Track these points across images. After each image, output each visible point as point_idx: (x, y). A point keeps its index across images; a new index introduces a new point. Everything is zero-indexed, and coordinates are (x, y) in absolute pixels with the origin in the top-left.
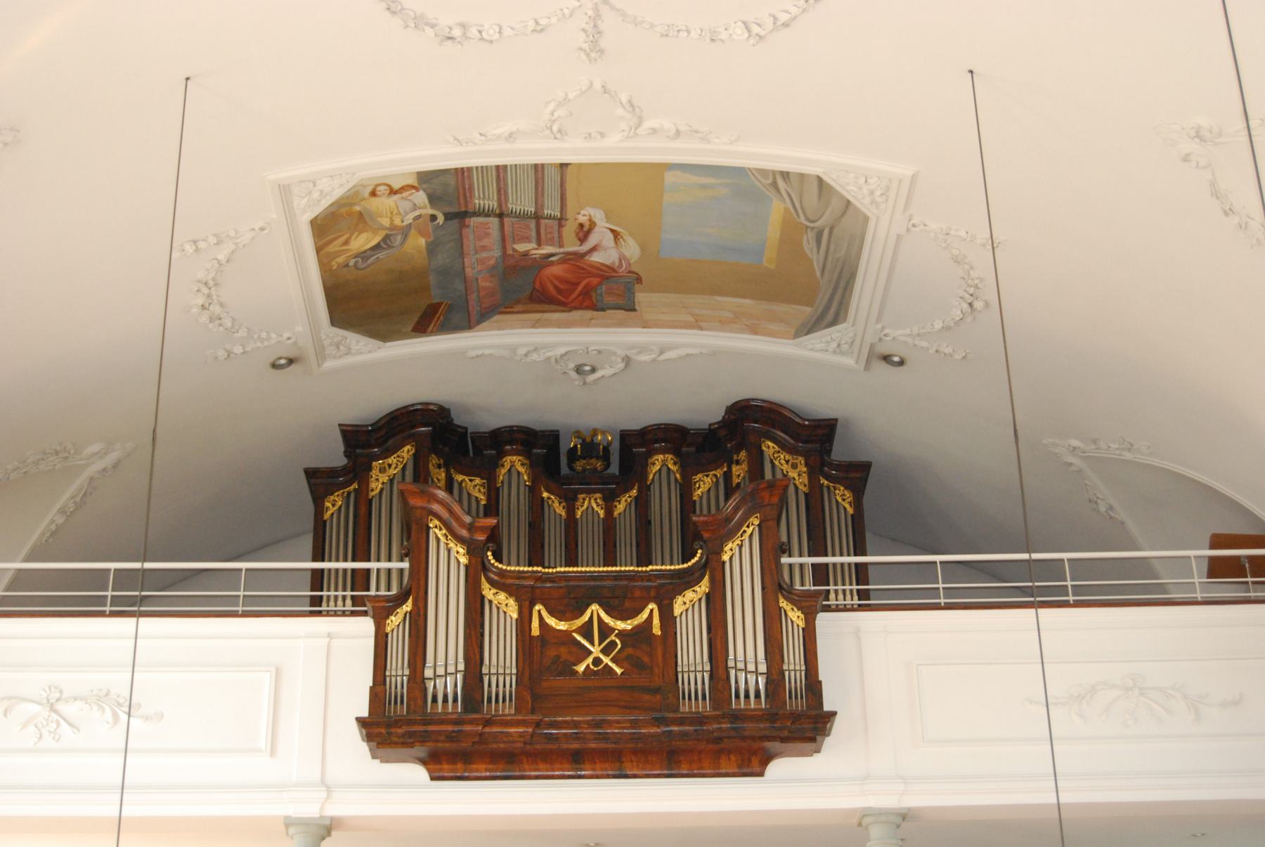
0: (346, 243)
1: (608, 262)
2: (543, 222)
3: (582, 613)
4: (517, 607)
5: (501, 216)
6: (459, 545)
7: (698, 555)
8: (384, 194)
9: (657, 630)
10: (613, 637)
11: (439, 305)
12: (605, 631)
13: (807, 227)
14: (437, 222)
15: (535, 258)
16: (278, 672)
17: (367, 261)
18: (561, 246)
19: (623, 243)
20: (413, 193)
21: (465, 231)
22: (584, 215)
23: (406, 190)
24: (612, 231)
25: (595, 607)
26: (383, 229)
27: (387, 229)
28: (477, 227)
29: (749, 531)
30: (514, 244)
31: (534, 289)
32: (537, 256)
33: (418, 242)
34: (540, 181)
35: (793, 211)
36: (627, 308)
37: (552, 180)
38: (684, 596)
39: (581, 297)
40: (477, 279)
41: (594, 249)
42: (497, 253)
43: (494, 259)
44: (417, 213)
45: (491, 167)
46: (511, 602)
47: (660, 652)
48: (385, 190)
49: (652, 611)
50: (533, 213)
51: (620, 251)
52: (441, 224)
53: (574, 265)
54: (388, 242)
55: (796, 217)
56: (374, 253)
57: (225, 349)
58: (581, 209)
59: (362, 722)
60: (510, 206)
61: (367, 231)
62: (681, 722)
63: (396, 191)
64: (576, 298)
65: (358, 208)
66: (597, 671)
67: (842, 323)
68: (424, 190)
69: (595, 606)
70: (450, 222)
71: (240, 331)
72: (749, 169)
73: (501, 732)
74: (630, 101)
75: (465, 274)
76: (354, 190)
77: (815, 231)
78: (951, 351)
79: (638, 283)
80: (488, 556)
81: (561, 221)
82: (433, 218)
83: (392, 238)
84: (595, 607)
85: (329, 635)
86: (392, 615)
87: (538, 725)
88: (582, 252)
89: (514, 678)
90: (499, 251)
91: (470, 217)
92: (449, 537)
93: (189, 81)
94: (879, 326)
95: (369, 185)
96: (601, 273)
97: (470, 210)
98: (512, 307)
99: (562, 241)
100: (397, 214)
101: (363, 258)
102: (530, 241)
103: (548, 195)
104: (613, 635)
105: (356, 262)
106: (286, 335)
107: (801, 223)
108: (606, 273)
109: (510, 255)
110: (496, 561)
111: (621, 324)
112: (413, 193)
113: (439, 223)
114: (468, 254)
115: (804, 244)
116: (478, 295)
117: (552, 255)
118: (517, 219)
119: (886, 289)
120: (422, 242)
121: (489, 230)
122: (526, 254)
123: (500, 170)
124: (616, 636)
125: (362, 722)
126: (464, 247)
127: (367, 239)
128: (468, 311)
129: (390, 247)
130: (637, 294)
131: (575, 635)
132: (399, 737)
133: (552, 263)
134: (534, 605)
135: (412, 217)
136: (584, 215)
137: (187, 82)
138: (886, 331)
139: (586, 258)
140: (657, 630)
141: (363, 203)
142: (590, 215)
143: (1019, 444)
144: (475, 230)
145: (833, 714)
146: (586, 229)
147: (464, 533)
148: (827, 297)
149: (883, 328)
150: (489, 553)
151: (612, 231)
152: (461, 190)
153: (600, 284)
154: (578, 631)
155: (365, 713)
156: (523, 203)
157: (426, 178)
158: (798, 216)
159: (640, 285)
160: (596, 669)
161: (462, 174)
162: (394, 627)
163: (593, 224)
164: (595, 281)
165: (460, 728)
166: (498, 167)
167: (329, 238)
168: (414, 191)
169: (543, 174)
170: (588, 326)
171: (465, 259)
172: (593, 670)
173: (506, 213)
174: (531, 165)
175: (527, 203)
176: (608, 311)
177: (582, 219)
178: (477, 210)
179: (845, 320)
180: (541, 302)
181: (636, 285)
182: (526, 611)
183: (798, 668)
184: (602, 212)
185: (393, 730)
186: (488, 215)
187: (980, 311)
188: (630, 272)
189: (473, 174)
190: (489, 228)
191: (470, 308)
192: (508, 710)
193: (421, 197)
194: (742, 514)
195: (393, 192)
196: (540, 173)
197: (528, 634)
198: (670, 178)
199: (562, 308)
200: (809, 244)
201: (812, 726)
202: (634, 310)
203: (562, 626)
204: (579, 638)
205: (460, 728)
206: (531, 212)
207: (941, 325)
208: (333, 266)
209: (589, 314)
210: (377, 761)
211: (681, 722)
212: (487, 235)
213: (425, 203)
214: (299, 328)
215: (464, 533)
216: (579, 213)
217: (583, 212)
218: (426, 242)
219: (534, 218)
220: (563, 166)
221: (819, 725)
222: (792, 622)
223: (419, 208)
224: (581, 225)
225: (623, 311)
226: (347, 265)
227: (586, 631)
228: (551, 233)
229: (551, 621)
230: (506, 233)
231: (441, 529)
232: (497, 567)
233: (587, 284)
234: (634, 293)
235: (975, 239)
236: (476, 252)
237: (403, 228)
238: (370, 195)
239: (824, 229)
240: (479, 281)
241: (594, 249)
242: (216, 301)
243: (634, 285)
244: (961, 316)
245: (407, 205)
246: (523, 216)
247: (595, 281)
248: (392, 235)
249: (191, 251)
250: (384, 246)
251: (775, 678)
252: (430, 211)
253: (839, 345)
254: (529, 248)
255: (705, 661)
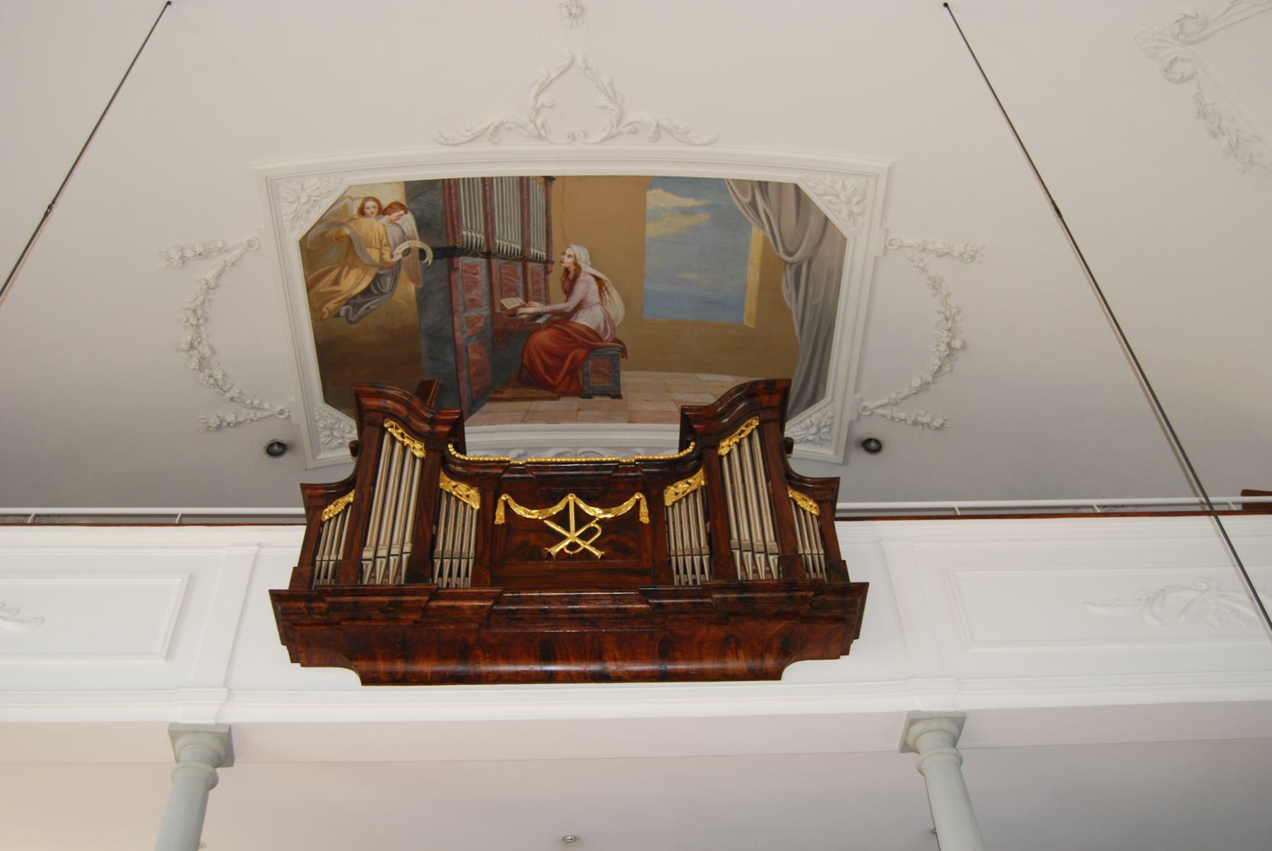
0: (336, 281)
1: (593, 327)
2: (531, 265)
3: (555, 503)
4: (479, 497)
5: (488, 255)
6: (416, 442)
7: (691, 447)
8: (372, 213)
9: (645, 519)
10: (592, 525)
11: (431, 383)
12: (582, 518)
13: (786, 263)
14: (425, 261)
15: (523, 319)
16: (192, 579)
17: (358, 310)
18: (548, 303)
19: (607, 297)
20: (401, 215)
21: (456, 276)
22: (569, 256)
23: (395, 211)
24: (598, 279)
25: (571, 498)
26: (373, 266)
27: (377, 266)
28: (465, 271)
29: (748, 431)
30: (502, 297)
31: (523, 364)
32: (525, 316)
33: (407, 289)
34: (526, 203)
35: (773, 244)
36: (613, 393)
37: (537, 192)
38: (676, 487)
39: (568, 378)
40: (467, 348)
41: (579, 307)
42: (485, 311)
43: (483, 320)
44: (405, 246)
45: (478, 178)
46: (473, 492)
47: (648, 539)
48: (374, 207)
49: (638, 502)
50: (520, 251)
51: (605, 309)
52: (430, 263)
53: (561, 330)
54: (379, 285)
55: (774, 248)
56: (366, 300)
57: (218, 417)
58: (567, 247)
59: (277, 597)
60: (497, 241)
61: (356, 267)
62: (676, 594)
63: (385, 210)
64: (562, 380)
65: (347, 231)
66: (574, 555)
67: (821, 399)
68: (413, 213)
69: (572, 496)
70: (439, 262)
71: (231, 390)
72: (727, 180)
73: (452, 607)
74: (611, 84)
75: (455, 341)
76: (341, 204)
77: (794, 267)
78: (929, 420)
79: (622, 357)
80: (448, 448)
81: (547, 263)
82: (422, 253)
83: (381, 279)
84: (571, 498)
85: (260, 545)
86: (331, 504)
87: (498, 599)
88: (568, 310)
89: (471, 561)
90: (487, 307)
91: (459, 256)
92: (406, 435)
93: (168, 6)
94: (857, 396)
95: (357, 199)
96: (588, 342)
97: (458, 245)
98: (502, 392)
99: (549, 295)
100: (386, 246)
101: (354, 305)
102: (517, 296)
103: (534, 225)
104: (594, 521)
105: (347, 312)
106: (279, 408)
107: (780, 258)
108: (590, 341)
109: (499, 314)
110: (458, 452)
111: (608, 418)
112: (401, 215)
113: (428, 262)
114: (457, 311)
115: (783, 289)
116: (469, 373)
117: (539, 315)
118: (504, 261)
119: (866, 328)
120: (411, 288)
121: (477, 276)
122: (513, 313)
123: (486, 182)
124: (597, 523)
125: (276, 596)
126: (454, 299)
127: (357, 278)
128: (459, 397)
129: (381, 293)
130: (623, 374)
131: (546, 522)
132: (321, 614)
133: (539, 328)
134: (500, 496)
135: (401, 251)
136: (569, 256)
137: (166, 7)
138: (865, 403)
139: (572, 319)
140: (645, 519)
141: (351, 224)
142: (575, 257)
143: (1064, 217)
144: (464, 276)
145: (863, 588)
146: (571, 276)
147: (426, 427)
148: (806, 364)
149: (862, 400)
150: (450, 446)
151: (598, 279)
152: (448, 215)
153: (586, 358)
154: (552, 518)
155: (284, 584)
156: (510, 238)
157: (416, 190)
158: (778, 251)
159: (624, 359)
160: (571, 553)
161: (449, 187)
162: (331, 515)
163: (578, 269)
164: (581, 353)
165: (399, 598)
166: (484, 179)
167: (319, 271)
168: (402, 212)
169: (528, 194)
170: (576, 420)
171: (455, 319)
172: (569, 554)
173: (493, 251)
174: (517, 177)
175: (513, 239)
176: (597, 399)
177: (568, 261)
178: (465, 247)
179: (823, 396)
180: (529, 384)
181: (621, 359)
182: (490, 500)
183: (815, 551)
184: (586, 250)
185: (314, 605)
186: (475, 255)
187: (958, 350)
188: (615, 340)
189: (460, 192)
190: (477, 274)
191: (461, 391)
192: (464, 583)
193: (408, 222)
194: (739, 406)
195: (382, 212)
196: (525, 193)
197: (490, 522)
198: (655, 198)
199: (549, 394)
200: (788, 289)
201: (839, 598)
202: (619, 396)
203: (534, 514)
204: (553, 526)
205: (399, 598)
206: (518, 250)
207: (920, 382)
208: (325, 313)
209: (575, 402)
210: (298, 665)
211: (676, 594)
212: (476, 282)
213: (413, 230)
214: (292, 399)
215: (426, 427)
216: (564, 253)
217: (568, 251)
218: (416, 288)
219: (521, 260)
220: (549, 180)
221: (848, 599)
222: (804, 511)
223: (409, 239)
224: (567, 271)
225: (608, 399)
226: (338, 315)
227: (562, 519)
228: (538, 282)
229: (520, 511)
230: (494, 281)
231: (397, 428)
232: (459, 459)
233: (574, 358)
234: (618, 372)
235: (952, 250)
236: (465, 310)
237: (392, 267)
238: (359, 214)
239: (803, 264)
240: (470, 350)
241: (579, 307)
242: (205, 343)
243: (619, 359)
244: (940, 363)
245: (394, 233)
246: (509, 257)
247: (581, 353)
248: (381, 275)
249: (177, 257)
250: (375, 292)
251: (790, 559)
252: (418, 244)
253: (819, 430)
254: (515, 306)
255: (702, 545)
